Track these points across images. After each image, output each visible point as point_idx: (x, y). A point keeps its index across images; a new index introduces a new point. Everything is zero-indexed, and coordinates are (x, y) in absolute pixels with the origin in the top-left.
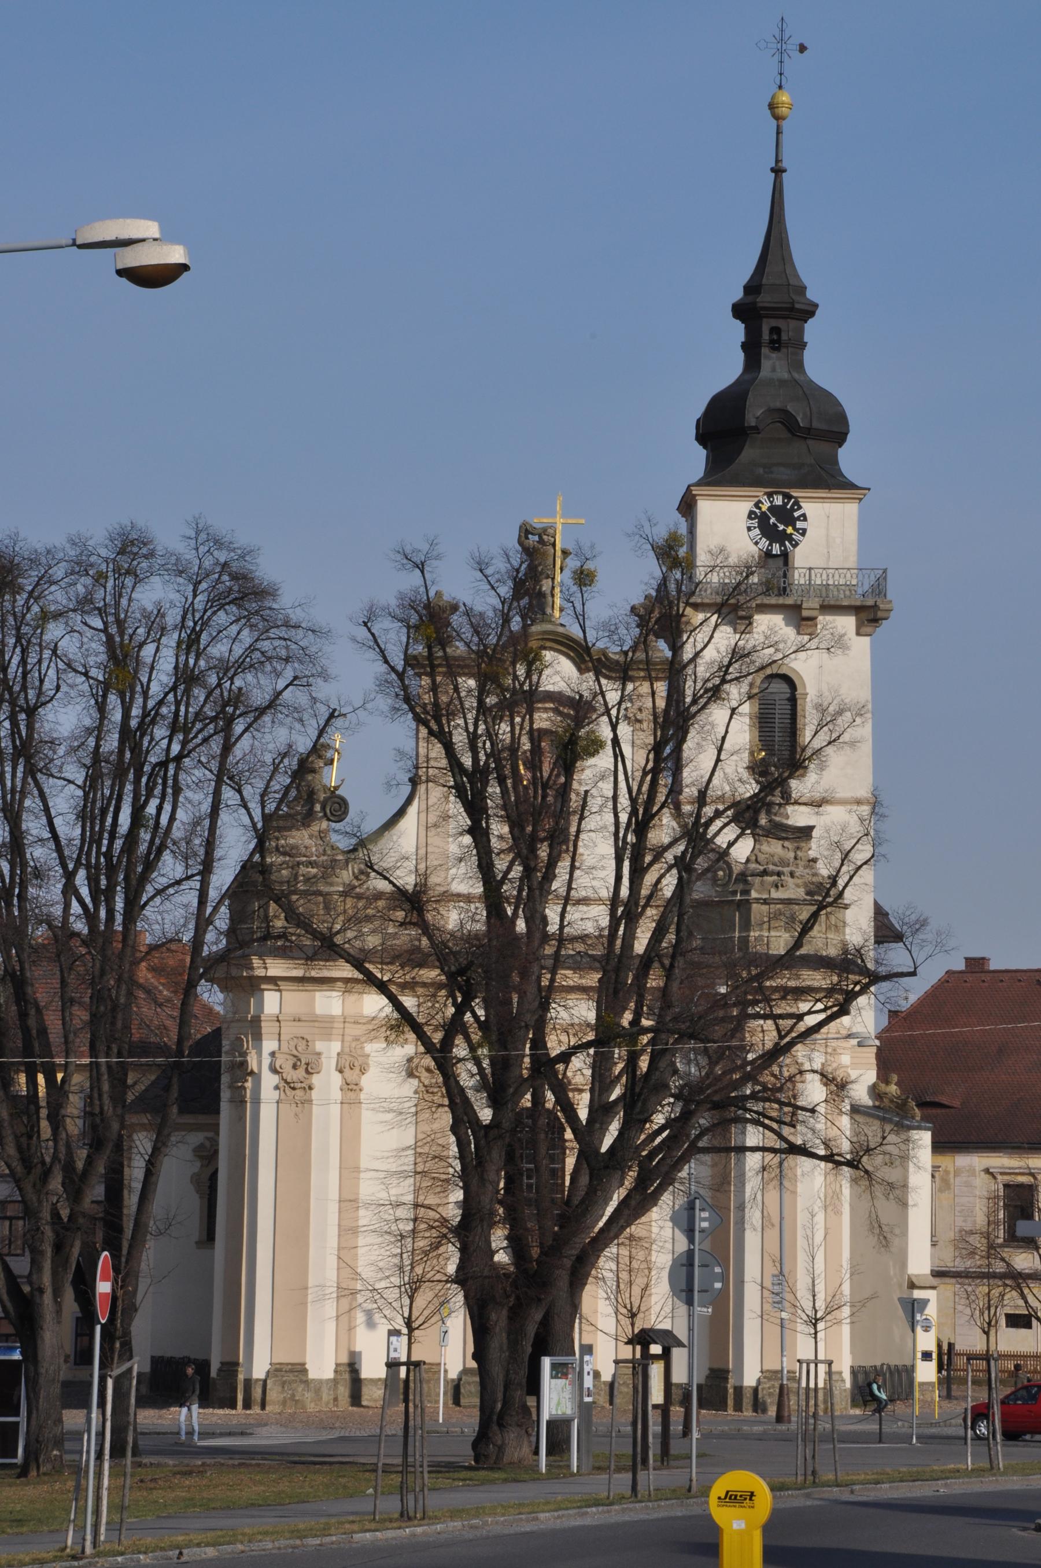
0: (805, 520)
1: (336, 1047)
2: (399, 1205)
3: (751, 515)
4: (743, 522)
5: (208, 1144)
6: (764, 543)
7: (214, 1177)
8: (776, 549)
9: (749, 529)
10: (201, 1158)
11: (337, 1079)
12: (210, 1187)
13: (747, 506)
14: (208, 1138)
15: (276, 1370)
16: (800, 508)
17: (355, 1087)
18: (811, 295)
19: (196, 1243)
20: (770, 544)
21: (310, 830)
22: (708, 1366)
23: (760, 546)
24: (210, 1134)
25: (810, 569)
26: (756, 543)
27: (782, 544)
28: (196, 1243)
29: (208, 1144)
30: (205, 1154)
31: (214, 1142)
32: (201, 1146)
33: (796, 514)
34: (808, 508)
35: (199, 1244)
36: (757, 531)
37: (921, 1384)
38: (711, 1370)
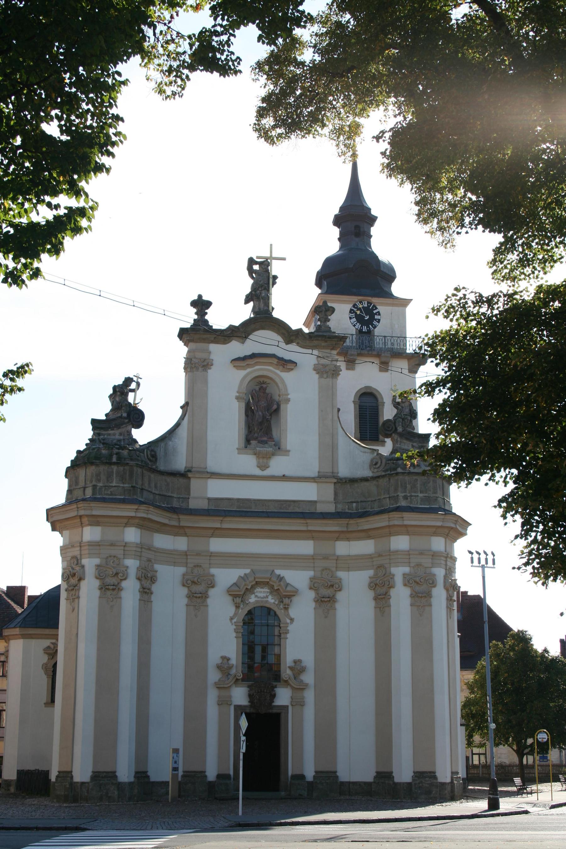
0: (379, 314)
1: (97, 561)
2: (88, 793)
3: (351, 311)
4: (347, 315)
5: (52, 646)
6: (358, 326)
7: (55, 665)
8: (365, 329)
9: (350, 318)
10: (49, 654)
11: (137, 585)
12: (53, 671)
13: (349, 306)
14: (52, 643)
16: (376, 308)
17: (148, 591)
18: (373, 213)
19: (45, 704)
20: (362, 326)
21: (120, 431)
22: (375, 771)
23: (356, 327)
24: (54, 641)
25: (385, 337)
26: (354, 326)
27: (368, 327)
28: (45, 704)
29: (52, 646)
30: (52, 652)
31: (55, 645)
32: (49, 647)
33: (375, 312)
34: (380, 308)
35: (46, 704)
36: (355, 320)
38: (377, 772)
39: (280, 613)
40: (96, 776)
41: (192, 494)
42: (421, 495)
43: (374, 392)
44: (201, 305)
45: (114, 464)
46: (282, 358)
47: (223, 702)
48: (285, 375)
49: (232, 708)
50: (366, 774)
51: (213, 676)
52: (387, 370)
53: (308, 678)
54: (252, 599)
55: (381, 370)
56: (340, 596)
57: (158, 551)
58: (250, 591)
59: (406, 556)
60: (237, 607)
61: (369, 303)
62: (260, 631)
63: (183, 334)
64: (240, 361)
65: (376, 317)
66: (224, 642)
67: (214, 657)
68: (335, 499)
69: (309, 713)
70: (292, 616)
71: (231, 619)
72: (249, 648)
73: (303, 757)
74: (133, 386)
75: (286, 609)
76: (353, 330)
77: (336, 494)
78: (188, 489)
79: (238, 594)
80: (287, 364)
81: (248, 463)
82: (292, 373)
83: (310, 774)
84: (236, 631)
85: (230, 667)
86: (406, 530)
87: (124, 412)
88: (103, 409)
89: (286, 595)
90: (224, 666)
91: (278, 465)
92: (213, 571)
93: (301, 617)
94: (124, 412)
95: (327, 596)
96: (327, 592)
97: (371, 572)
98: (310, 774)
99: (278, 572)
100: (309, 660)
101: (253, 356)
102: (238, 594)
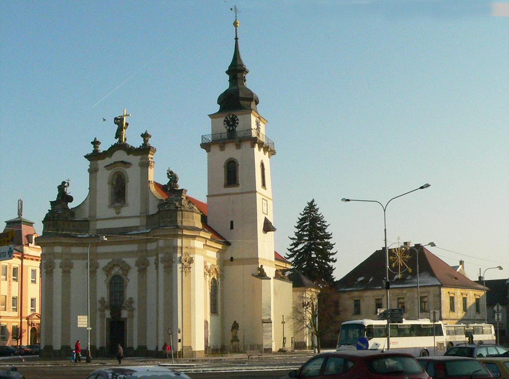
1: (60, 261)
3: (225, 121)
6: (228, 127)
13: (223, 119)
15: (46, 347)
25: (221, 134)
27: (232, 127)
34: (239, 117)
37: (265, 349)
39: (124, 277)
40: (63, 347)
41: (90, 228)
42: (169, 220)
43: (229, 160)
44: (96, 143)
45: (51, 220)
46: (111, 164)
47: (103, 316)
48: (127, 170)
49: (105, 319)
50: (154, 349)
51: (99, 306)
52: (240, 148)
53: (135, 305)
54: (113, 272)
55: (237, 149)
56: (72, 270)
57: (73, 255)
58: (112, 268)
59: (61, 255)
60: (107, 276)
61: (233, 115)
62: (117, 285)
63: (87, 157)
64: (108, 167)
65: (236, 121)
66: (103, 292)
67: (99, 298)
68: (147, 224)
69: (135, 319)
70: (129, 278)
71: (105, 281)
72: (111, 294)
73: (133, 340)
74: (66, 185)
75: (126, 275)
76: (225, 131)
77: (147, 222)
78: (89, 226)
79: (108, 270)
80: (126, 164)
81: (112, 212)
82: (129, 169)
83: (135, 347)
84: (107, 287)
85: (105, 302)
86: (61, 244)
87: (64, 197)
88: (54, 196)
89: (126, 269)
90: (102, 301)
91: (125, 211)
92: (73, 261)
93: (133, 277)
94: (64, 197)
95: (143, 268)
96: (67, 269)
97: (136, 259)
98: (135, 347)
99: (123, 259)
100: (135, 298)
101: (115, 163)
102: (108, 270)
